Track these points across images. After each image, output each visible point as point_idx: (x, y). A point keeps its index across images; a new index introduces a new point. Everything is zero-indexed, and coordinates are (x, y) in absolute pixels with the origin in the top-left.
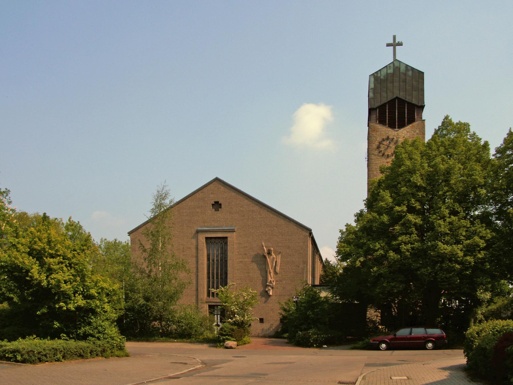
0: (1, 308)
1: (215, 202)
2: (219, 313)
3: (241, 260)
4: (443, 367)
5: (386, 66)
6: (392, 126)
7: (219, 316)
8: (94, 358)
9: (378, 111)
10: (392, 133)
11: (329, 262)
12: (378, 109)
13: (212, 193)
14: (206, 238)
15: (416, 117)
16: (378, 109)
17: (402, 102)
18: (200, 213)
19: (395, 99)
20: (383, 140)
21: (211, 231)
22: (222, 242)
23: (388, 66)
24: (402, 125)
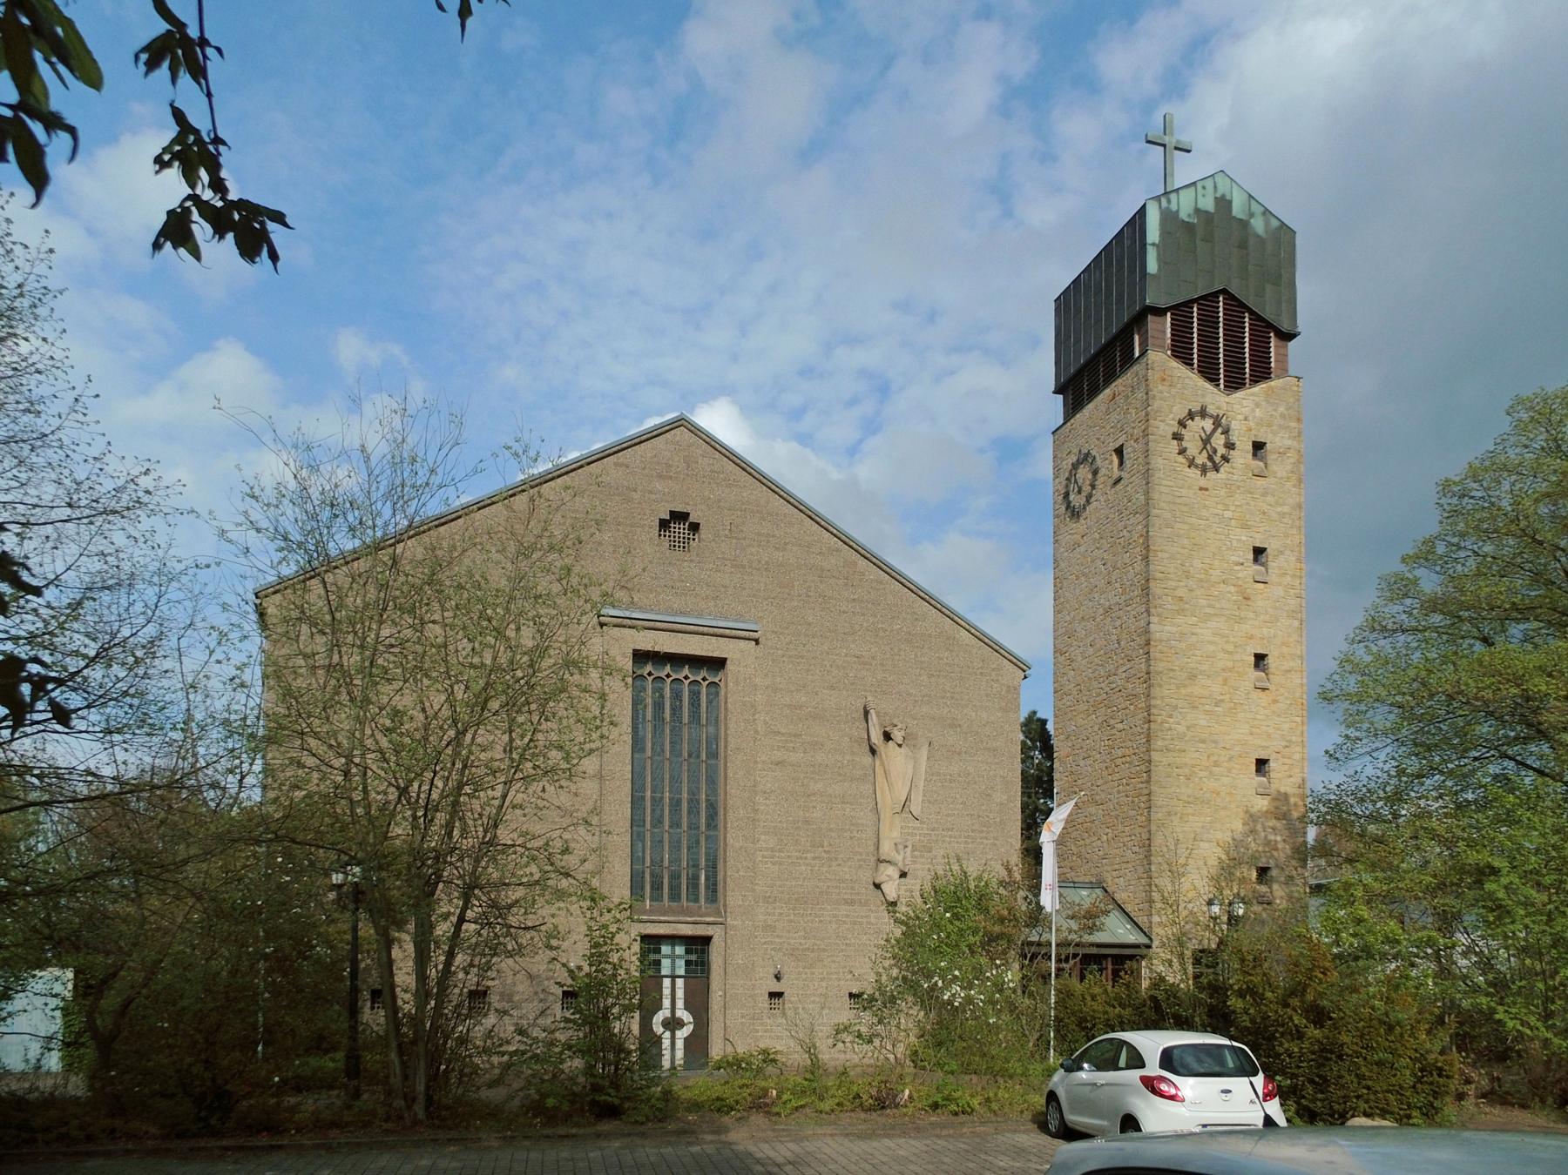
0: (15, 1063)
1: (672, 513)
2: (681, 971)
3: (778, 755)
4: (1090, 1140)
5: (1194, 184)
6: (1208, 372)
7: (680, 983)
8: (89, 772)
9: (1169, 319)
10: (1214, 397)
11: (52, 1094)
12: (1169, 314)
13: (660, 476)
14: (640, 657)
15: (1272, 365)
16: (1169, 314)
17: (1237, 306)
18: (611, 549)
19: (1215, 295)
20: (1191, 416)
21: (658, 625)
22: (699, 679)
23: (1199, 185)
24: (1235, 383)
